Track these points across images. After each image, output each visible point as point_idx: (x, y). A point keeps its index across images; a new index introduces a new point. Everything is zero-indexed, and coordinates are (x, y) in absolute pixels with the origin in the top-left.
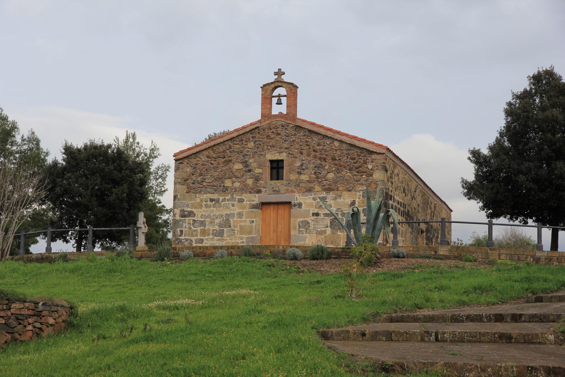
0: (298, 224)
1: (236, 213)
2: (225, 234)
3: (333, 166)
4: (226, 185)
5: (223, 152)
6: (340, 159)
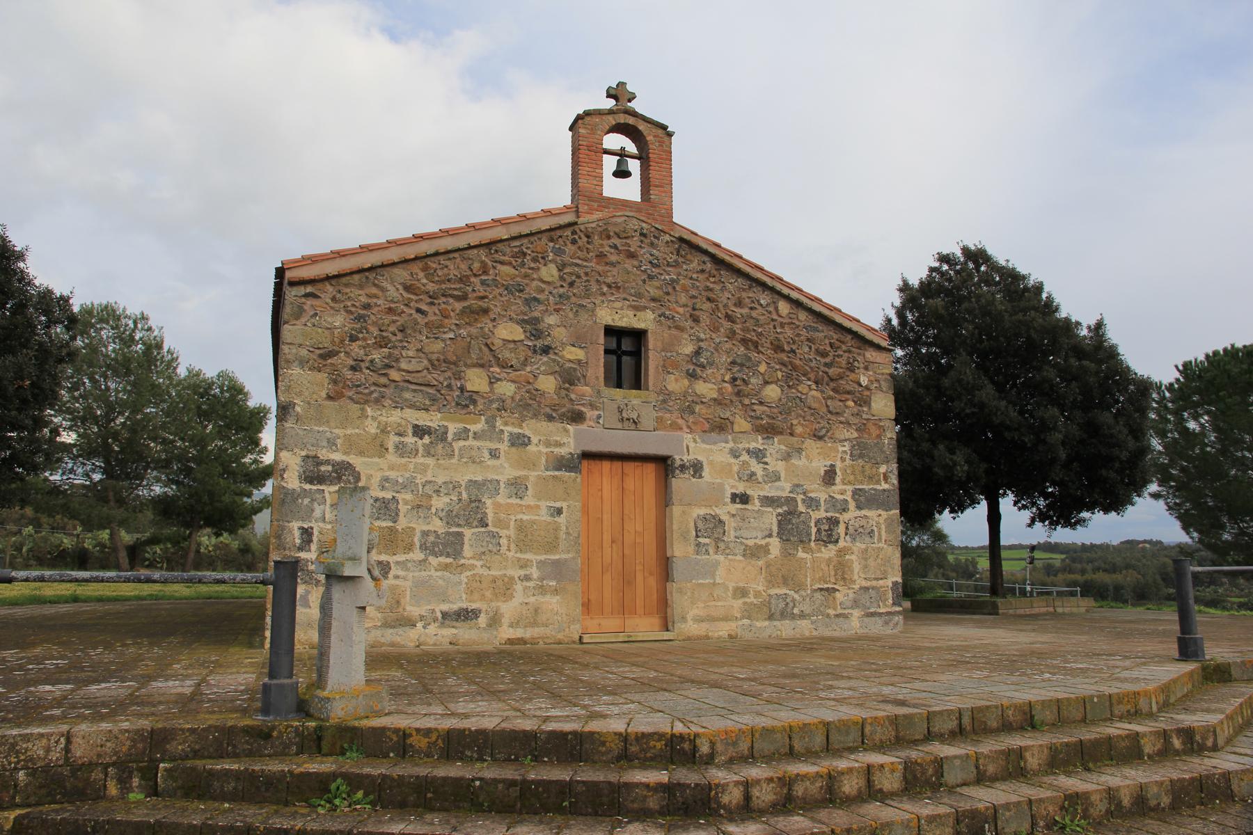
0: (692, 524)
1: (503, 478)
2: (466, 547)
3: (778, 367)
5: (461, 280)
6: (793, 351)
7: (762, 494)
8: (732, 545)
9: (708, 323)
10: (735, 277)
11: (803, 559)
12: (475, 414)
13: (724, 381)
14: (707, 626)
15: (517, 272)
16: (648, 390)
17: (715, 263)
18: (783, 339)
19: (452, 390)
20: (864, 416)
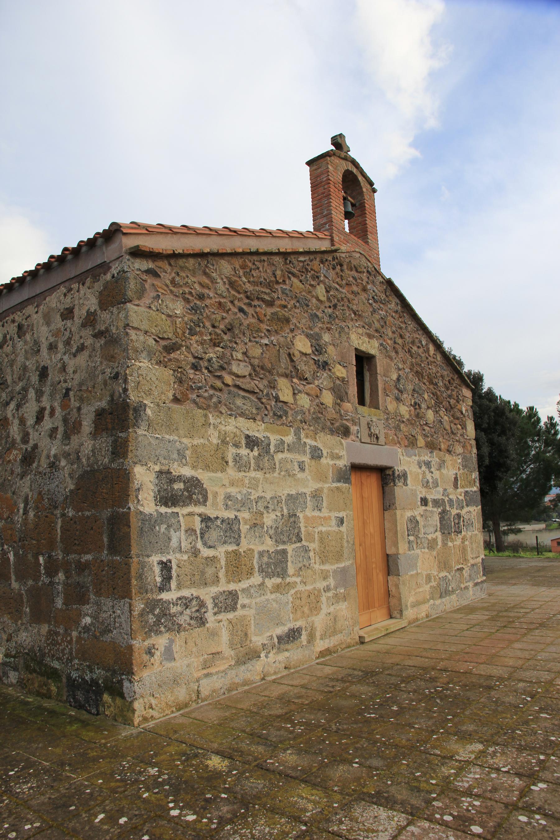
1: (308, 491)
16: (377, 408)
20: (466, 437)
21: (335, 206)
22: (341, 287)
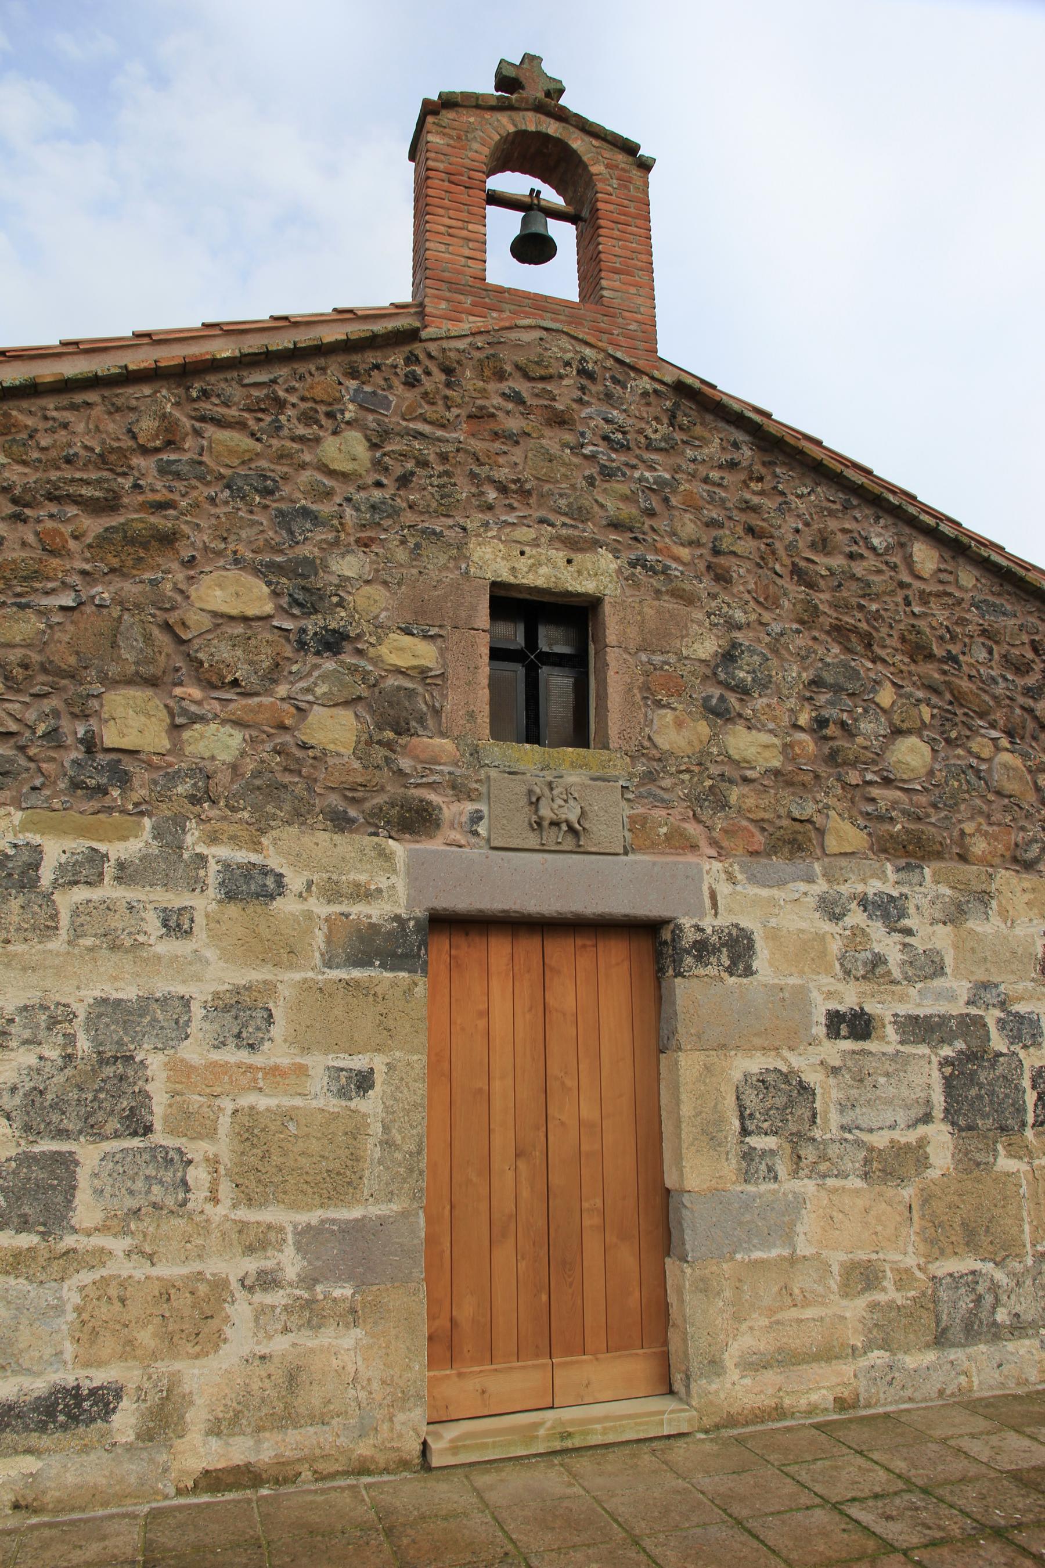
0: (730, 1101)
1: (200, 992)
2: (83, 1197)
3: (920, 694)
4: (110, 738)
5: (103, 460)
6: (952, 658)
7: (903, 1009)
8: (833, 1151)
9: (752, 586)
10: (808, 481)
11: (1008, 1175)
12: (124, 812)
13: (796, 727)
14: (779, 1379)
15: (259, 447)
17: (760, 448)
18: (928, 630)
19: (60, 746)
21: (443, 229)
22: (443, 426)
